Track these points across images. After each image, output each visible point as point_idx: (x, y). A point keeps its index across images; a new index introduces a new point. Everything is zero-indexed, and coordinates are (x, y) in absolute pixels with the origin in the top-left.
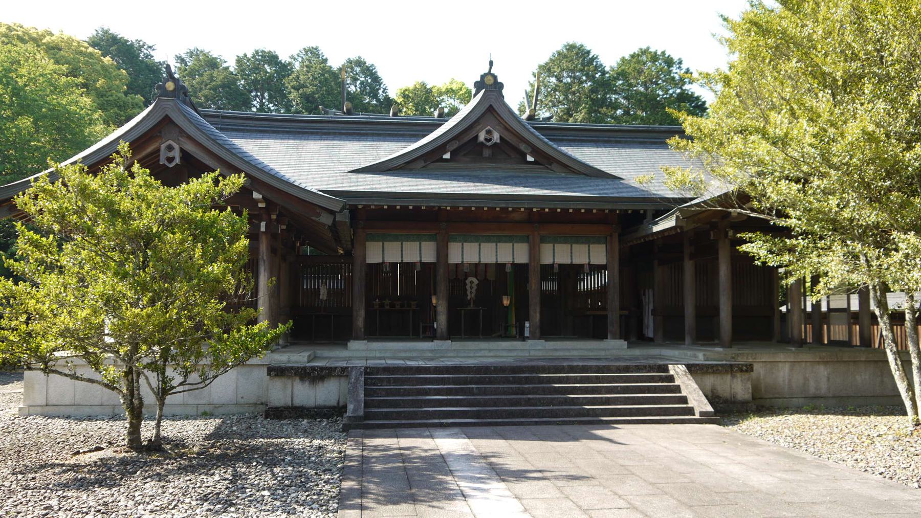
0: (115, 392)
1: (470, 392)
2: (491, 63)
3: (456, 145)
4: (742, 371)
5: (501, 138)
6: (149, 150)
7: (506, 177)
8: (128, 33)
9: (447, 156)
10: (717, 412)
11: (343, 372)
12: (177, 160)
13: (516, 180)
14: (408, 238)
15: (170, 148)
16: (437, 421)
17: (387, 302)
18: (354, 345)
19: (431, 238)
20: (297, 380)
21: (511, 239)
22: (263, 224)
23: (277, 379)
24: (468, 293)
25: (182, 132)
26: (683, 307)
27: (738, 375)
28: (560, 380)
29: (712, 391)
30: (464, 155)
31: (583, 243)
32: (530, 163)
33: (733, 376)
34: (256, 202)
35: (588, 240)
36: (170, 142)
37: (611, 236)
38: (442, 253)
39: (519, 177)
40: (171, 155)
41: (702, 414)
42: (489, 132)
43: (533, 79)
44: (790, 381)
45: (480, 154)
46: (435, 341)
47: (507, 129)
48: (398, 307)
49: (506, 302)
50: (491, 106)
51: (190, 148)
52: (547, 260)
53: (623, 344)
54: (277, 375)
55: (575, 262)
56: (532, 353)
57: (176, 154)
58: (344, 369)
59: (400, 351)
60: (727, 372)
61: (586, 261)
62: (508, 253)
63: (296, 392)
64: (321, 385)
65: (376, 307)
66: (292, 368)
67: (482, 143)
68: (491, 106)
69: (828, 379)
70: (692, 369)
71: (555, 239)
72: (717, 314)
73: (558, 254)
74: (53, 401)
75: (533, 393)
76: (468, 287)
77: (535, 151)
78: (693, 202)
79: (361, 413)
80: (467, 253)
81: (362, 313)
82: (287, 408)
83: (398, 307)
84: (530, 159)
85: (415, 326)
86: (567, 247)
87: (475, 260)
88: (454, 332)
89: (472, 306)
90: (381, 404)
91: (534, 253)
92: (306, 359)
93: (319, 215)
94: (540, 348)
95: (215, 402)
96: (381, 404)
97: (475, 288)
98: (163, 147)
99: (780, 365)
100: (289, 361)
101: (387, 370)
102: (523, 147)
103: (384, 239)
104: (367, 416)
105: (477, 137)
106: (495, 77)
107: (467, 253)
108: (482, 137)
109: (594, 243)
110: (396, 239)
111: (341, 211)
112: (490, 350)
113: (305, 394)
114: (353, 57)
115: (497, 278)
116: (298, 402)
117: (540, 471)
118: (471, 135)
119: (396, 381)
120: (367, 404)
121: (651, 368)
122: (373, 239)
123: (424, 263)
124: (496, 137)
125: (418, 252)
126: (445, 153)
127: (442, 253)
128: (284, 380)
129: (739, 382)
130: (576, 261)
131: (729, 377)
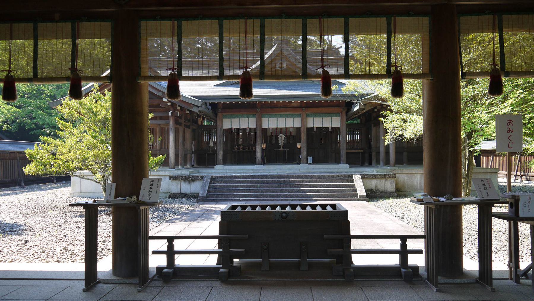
0: (99, 184)
1: (257, 187)
4: (390, 177)
7: (287, 86)
10: (368, 196)
13: (293, 87)
14: (243, 117)
17: (241, 147)
18: (217, 167)
19: (254, 116)
20: (183, 181)
21: (292, 116)
22: (170, 112)
23: (174, 181)
24: (280, 142)
26: (379, 147)
27: (389, 179)
28: (299, 182)
31: (328, 117)
33: (386, 180)
34: (166, 103)
35: (331, 115)
37: (342, 113)
38: (259, 123)
39: (295, 85)
41: (360, 196)
48: (247, 150)
52: (310, 125)
53: (348, 166)
54: (174, 179)
56: (301, 170)
58: (202, 177)
59: (238, 170)
60: (382, 178)
61: (330, 126)
62: (291, 123)
63: (182, 187)
65: (236, 150)
66: (180, 176)
70: (363, 177)
71: (314, 115)
73: (317, 122)
74: (83, 191)
75: (285, 187)
76: (279, 139)
78: (372, 95)
79: (205, 195)
80: (271, 123)
81: (221, 152)
82: (178, 194)
83: (247, 150)
85: (245, 157)
87: (275, 126)
89: (282, 149)
90: (215, 192)
92: (188, 173)
93: (193, 108)
94: (305, 168)
96: (215, 192)
97: (283, 139)
99: (415, 175)
101: (221, 177)
103: (231, 117)
104: (207, 197)
107: (271, 123)
111: (201, 106)
112: (280, 169)
113: (186, 188)
115: (293, 136)
116: (183, 192)
119: (224, 182)
121: (345, 176)
122: (226, 117)
125: (247, 123)
127: (259, 123)
128: (177, 181)
129: (389, 183)
130: (325, 126)
131: (384, 180)
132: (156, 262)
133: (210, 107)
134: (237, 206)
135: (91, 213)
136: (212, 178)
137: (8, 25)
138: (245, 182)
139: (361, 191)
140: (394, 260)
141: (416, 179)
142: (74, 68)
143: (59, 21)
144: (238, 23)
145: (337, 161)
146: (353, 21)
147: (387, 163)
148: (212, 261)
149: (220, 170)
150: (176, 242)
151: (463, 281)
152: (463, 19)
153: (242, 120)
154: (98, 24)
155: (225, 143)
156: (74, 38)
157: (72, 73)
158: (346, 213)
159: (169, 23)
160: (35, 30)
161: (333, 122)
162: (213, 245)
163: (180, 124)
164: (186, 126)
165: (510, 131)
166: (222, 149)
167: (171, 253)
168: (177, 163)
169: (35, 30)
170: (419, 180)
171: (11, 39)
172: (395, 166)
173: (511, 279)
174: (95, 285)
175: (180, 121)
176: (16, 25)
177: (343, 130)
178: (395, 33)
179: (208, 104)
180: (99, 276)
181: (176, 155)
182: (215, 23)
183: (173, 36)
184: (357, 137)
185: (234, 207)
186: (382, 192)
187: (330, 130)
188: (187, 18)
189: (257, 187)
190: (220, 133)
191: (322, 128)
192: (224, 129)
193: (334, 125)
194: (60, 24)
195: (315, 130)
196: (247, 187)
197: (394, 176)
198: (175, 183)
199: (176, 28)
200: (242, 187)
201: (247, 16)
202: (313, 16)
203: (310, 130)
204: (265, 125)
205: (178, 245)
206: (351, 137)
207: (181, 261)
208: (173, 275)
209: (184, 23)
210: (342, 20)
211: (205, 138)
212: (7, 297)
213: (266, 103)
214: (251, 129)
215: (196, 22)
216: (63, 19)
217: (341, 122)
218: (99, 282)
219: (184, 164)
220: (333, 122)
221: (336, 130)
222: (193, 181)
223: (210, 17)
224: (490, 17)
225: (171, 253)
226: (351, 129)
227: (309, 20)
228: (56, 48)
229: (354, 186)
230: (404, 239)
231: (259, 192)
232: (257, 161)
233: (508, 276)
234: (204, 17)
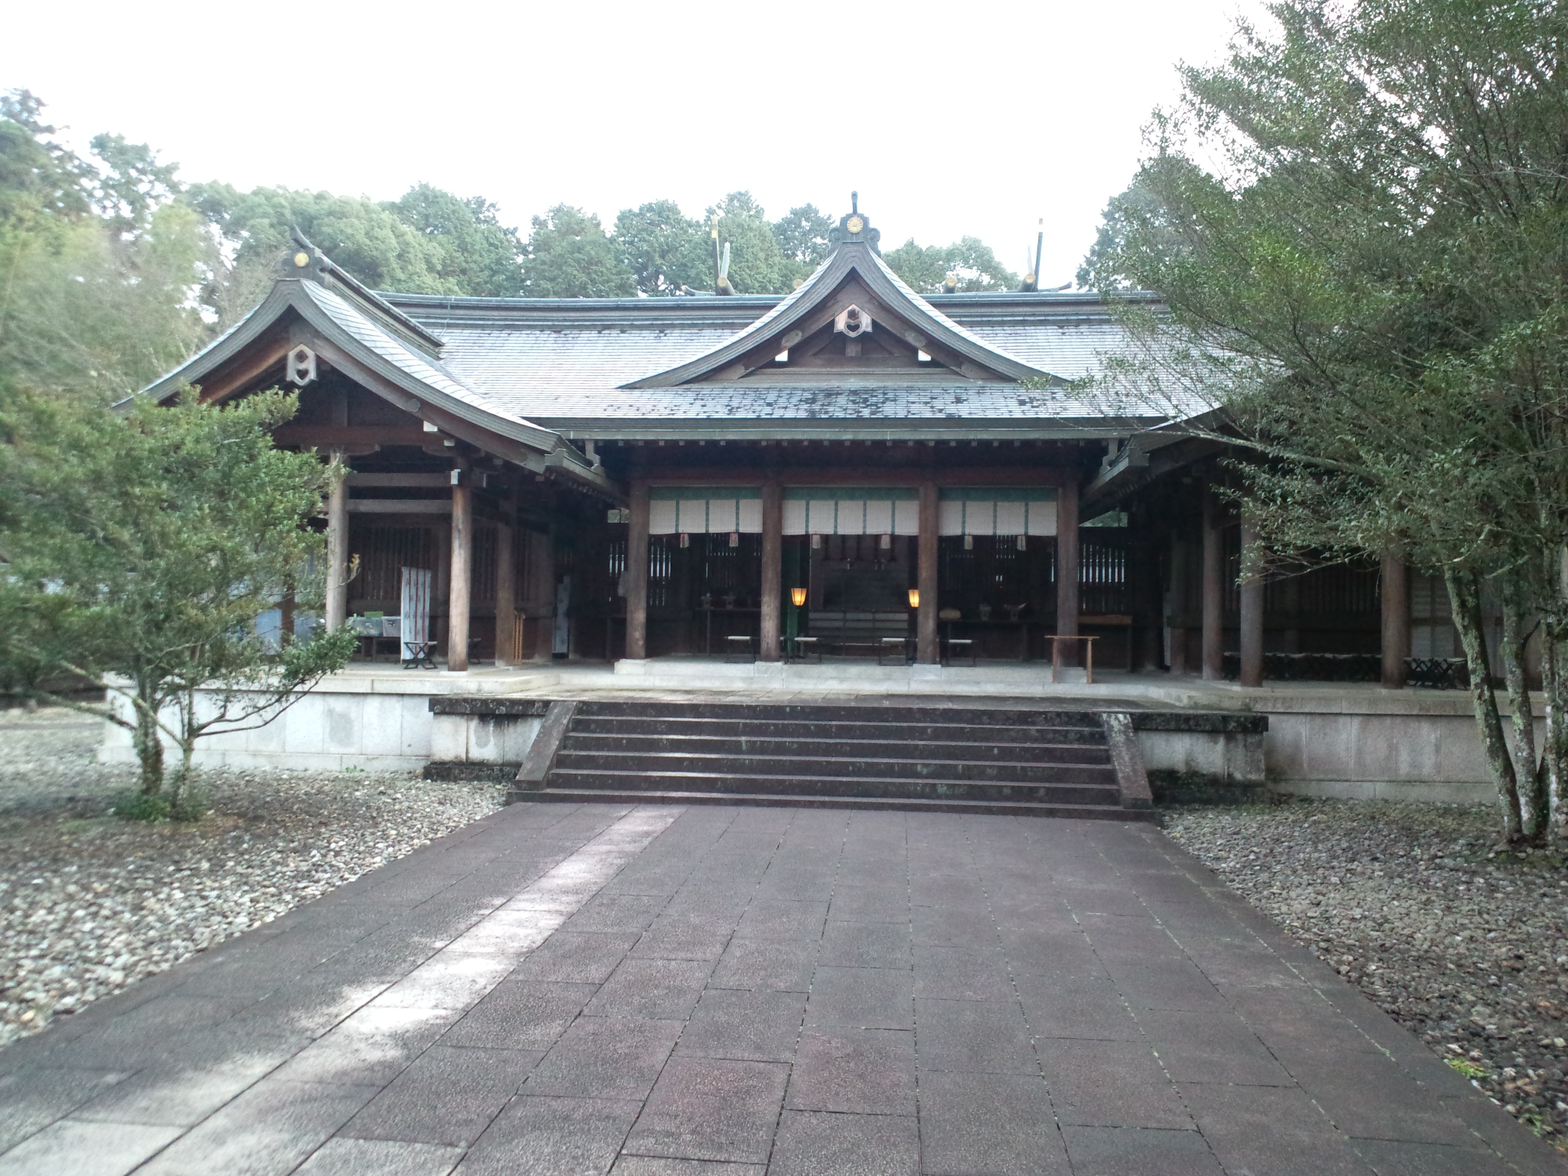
1: (736, 748)
2: (854, 196)
3: (796, 338)
5: (874, 323)
6: (272, 360)
8: (459, 187)
9: (783, 357)
12: (312, 375)
15: (301, 357)
16: (658, 794)
19: (755, 493)
21: (736, 494)
25: (317, 334)
29: (1187, 763)
30: (815, 354)
32: (924, 364)
36: (302, 347)
40: (302, 366)
42: (853, 315)
43: (1102, 222)
44: (1360, 752)
45: (843, 352)
46: (758, 664)
47: (885, 308)
49: (914, 600)
50: (853, 271)
51: (329, 355)
54: (443, 713)
55: (712, 530)
57: (310, 365)
61: (1021, 531)
64: (511, 729)
65: (707, 607)
67: (841, 333)
68: (853, 271)
69: (1437, 749)
71: (679, 494)
73: (973, 520)
77: (932, 344)
80: (816, 519)
84: (923, 357)
86: (1018, 508)
88: (790, 653)
91: (774, 516)
95: (369, 751)
98: (292, 355)
99: (1341, 720)
100: (479, 691)
102: (911, 338)
105: (832, 324)
106: (865, 221)
107: (816, 519)
108: (841, 323)
109: (745, 497)
110: (697, 494)
114: (800, 205)
120: (560, 761)
123: (900, 537)
124: (866, 322)
125: (733, 518)
126: (779, 351)
127: (774, 516)
130: (872, 530)
133: (596, 459)
136: (584, 707)
141: (1344, 736)
147: (1230, 669)
149: (636, 678)
153: (1004, 507)
161: (1041, 520)
166: (643, 604)
170: (1353, 737)
172: (1259, 684)
177: (1067, 552)
179: (590, 448)
184: (1117, 575)
187: (1021, 545)
189: (736, 748)
191: (835, 535)
192: (651, 536)
195: (968, 544)
197: (1255, 725)
198: (447, 724)
203: (950, 546)
206: (1091, 575)
214: (744, 537)
220: (1041, 520)
221: (1041, 547)
226: (1093, 542)
229: (1108, 760)
232: (764, 646)
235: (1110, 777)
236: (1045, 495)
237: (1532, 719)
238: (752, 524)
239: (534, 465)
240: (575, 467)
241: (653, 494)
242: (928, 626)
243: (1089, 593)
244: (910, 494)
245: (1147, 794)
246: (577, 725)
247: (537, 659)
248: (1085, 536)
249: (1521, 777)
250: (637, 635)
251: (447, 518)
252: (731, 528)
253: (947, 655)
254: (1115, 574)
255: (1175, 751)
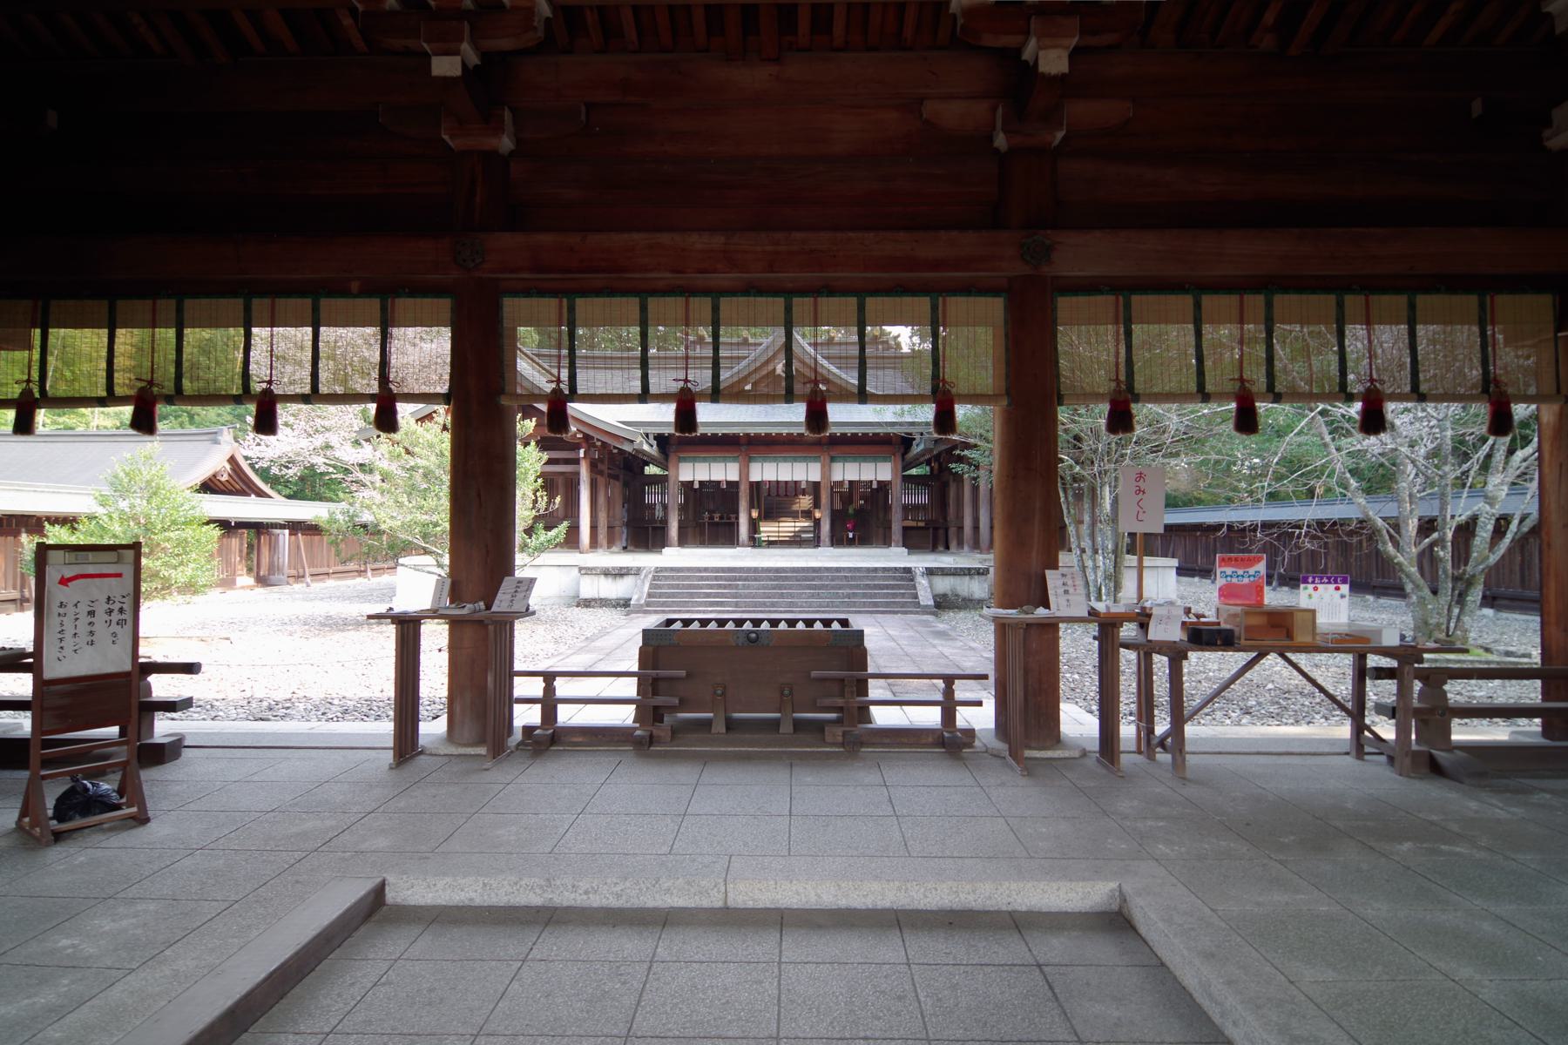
1: (737, 587)
11: (637, 572)
14: (715, 460)
19: (735, 459)
21: (805, 459)
35: (875, 458)
58: (639, 569)
71: (845, 458)
72: (680, 528)
80: (767, 471)
85: (721, 532)
86: (871, 466)
104: (648, 604)
107: (767, 471)
110: (855, 459)
117: (30, 368)
118: (770, 368)
120: (650, 595)
122: (685, 460)
127: (744, 472)
132: (526, 716)
134: (674, 621)
135: (408, 628)
136: (658, 570)
137: (149, 302)
138: (716, 578)
139: (926, 599)
140: (930, 717)
142: (384, 378)
143: (355, 296)
144: (674, 304)
145: (886, 542)
146: (1422, 300)
147: (976, 545)
148: (624, 716)
149: (675, 556)
150: (958, 685)
151: (1066, 754)
152: (1064, 304)
154: (427, 302)
155: (683, 509)
156: (1126, 321)
157: (380, 386)
158: (860, 634)
159: (552, 302)
160: (316, 309)
161: (879, 471)
162: (629, 688)
163: (601, 473)
164: (610, 476)
165: (1140, 491)
167: (549, 703)
168: (594, 544)
169: (316, 309)
171: (154, 327)
173: (1139, 752)
174: (413, 757)
175: (600, 466)
176: (281, 302)
178: (1493, 324)
180: (421, 742)
181: (594, 528)
182: (632, 304)
183: (1117, 322)
185: (670, 622)
186: (964, 599)
188: (585, 293)
189: (737, 587)
190: (673, 488)
193: (730, 478)
194: (359, 301)
196: (720, 586)
199: (565, 310)
200: (711, 587)
201: (688, 291)
202: (803, 292)
203: (756, 487)
204: (837, 476)
205: (563, 688)
206: (906, 500)
207: (567, 715)
208: (551, 740)
209: (579, 302)
210: (853, 301)
211: (631, 500)
212: (256, 778)
213: (757, 436)
215: (601, 300)
216: (367, 291)
217: (894, 473)
218: (421, 753)
219: (611, 542)
220: (879, 471)
221: (884, 486)
222: (622, 575)
223: (625, 292)
224: (1111, 298)
225: (549, 703)
227: (796, 300)
228: (351, 343)
230: (949, 680)
231: (740, 596)
233: (1134, 748)
234: (612, 292)
235: (916, 597)
236: (885, 460)
237: (1096, 567)
238: (733, 475)
239: (627, 448)
240: (646, 447)
241: (680, 460)
242: (826, 527)
243: (906, 509)
244: (816, 459)
245: (931, 603)
246: (654, 578)
247: (614, 549)
248: (907, 479)
249: (1092, 589)
250: (673, 530)
251: (578, 474)
252: (872, 478)
253: (838, 540)
254: (922, 498)
255: (944, 585)
